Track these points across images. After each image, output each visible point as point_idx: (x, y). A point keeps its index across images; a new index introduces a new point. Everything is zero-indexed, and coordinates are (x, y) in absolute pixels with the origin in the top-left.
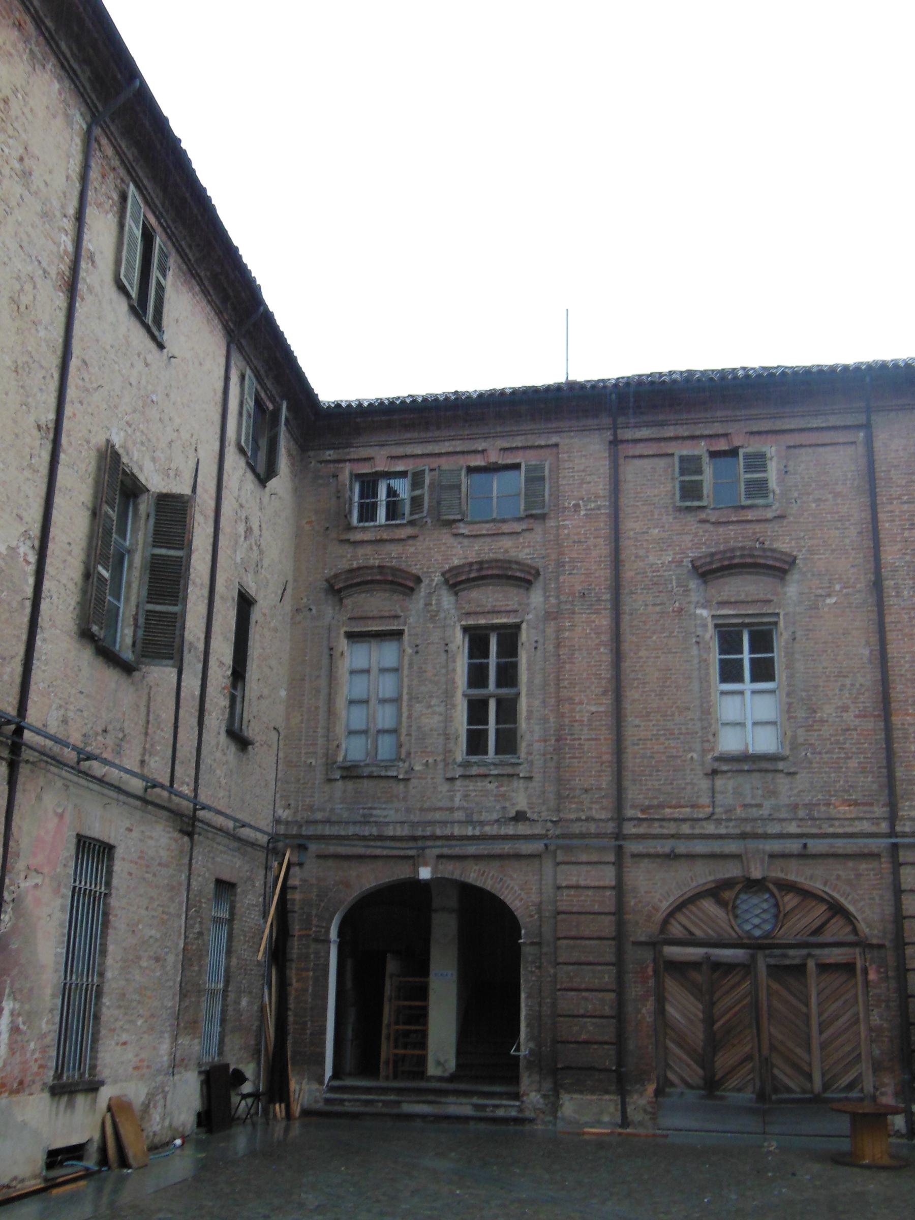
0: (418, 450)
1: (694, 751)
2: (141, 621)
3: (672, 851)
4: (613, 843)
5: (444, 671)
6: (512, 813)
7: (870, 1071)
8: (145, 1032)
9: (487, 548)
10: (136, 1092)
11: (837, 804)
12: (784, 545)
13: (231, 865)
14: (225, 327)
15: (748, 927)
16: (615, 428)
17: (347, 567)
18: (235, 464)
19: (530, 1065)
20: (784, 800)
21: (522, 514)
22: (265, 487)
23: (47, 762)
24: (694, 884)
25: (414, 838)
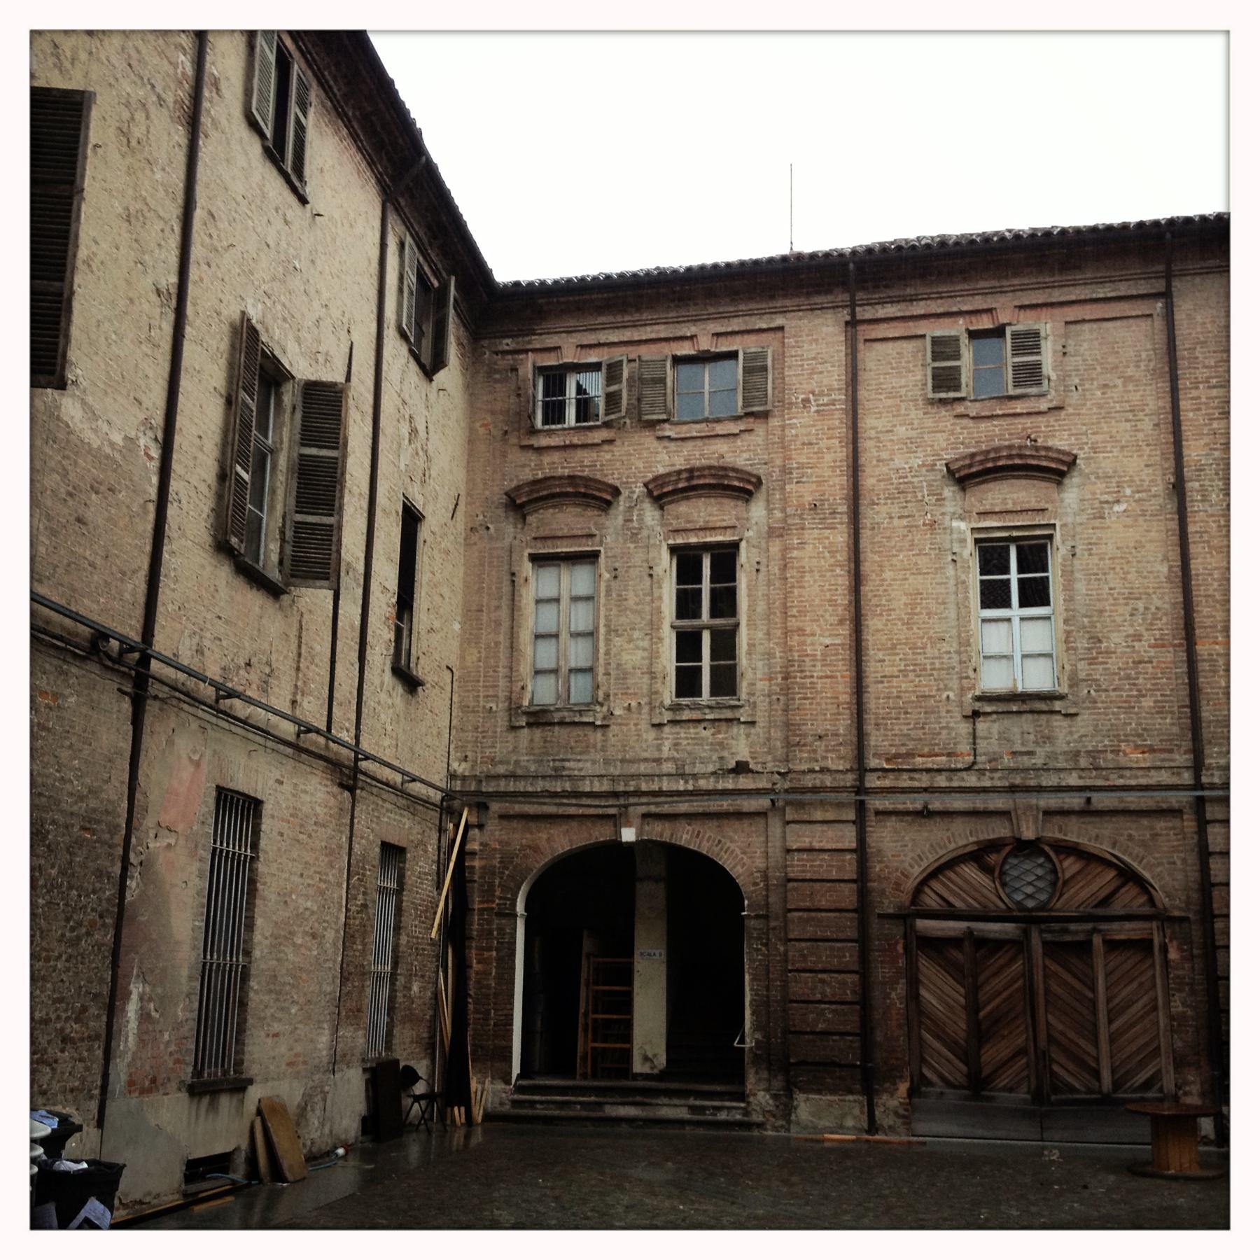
0: (614, 337)
1: (951, 689)
2: (289, 534)
3: (926, 807)
4: (853, 797)
5: (648, 599)
6: (732, 765)
7: (1171, 1068)
8: (300, 1022)
9: (697, 453)
10: (290, 1092)
11: (1128, 751)
12: (1061, 442)
13: (400, 826)
14: (380, 182)
15: (1018, 897)
16: (853, 306)
17: (531, 478)
18: (396, 351)
19: (757, 1060)
20: (1061, 745)
21: (740, 412)
22: (431, 380)
23: (179, 699)
24: (953, 846)
25: (615, 795)
